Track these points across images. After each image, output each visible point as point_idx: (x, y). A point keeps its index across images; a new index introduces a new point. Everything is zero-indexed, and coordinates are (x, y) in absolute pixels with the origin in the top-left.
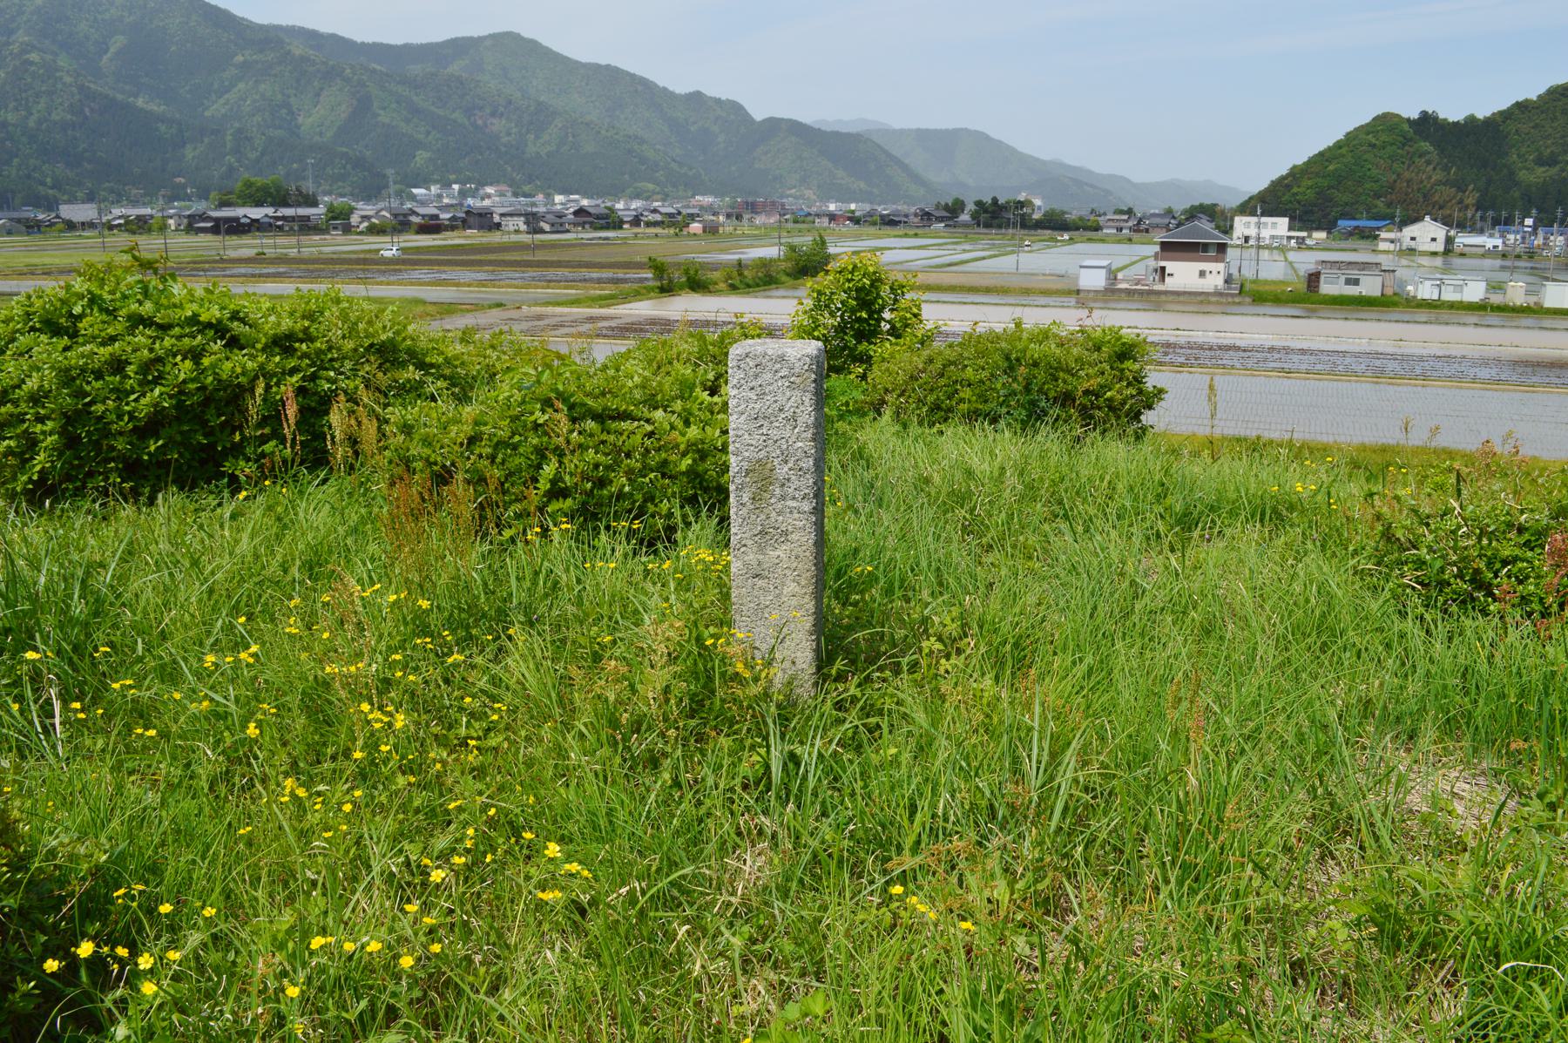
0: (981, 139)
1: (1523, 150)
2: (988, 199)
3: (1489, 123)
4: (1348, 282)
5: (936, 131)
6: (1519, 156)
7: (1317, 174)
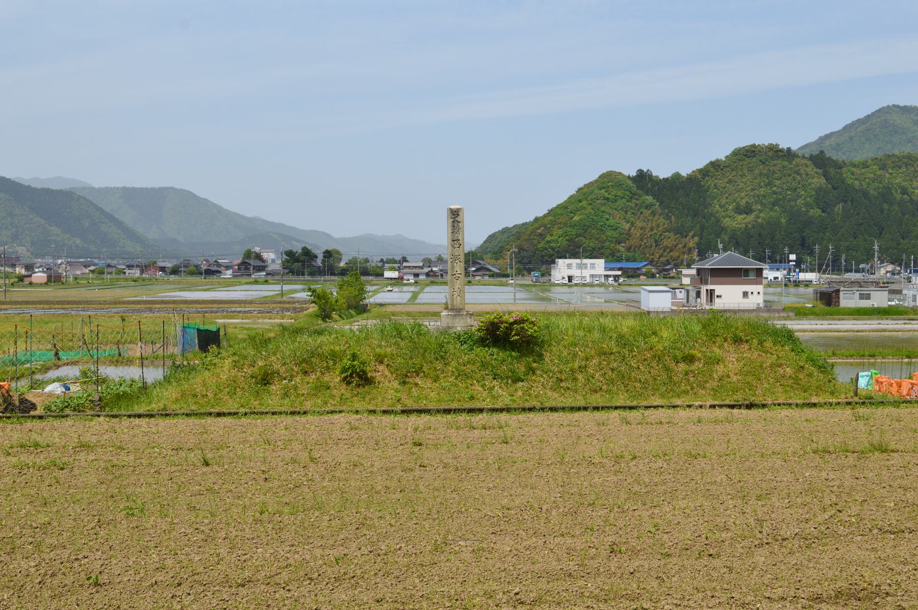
0: (188, 197)
1: (723, 201)
2: (298, 248)
3: (691, 179)
4: (862, 297)
5: (142, 190)
6: (720, 206)
7: (565, 224)
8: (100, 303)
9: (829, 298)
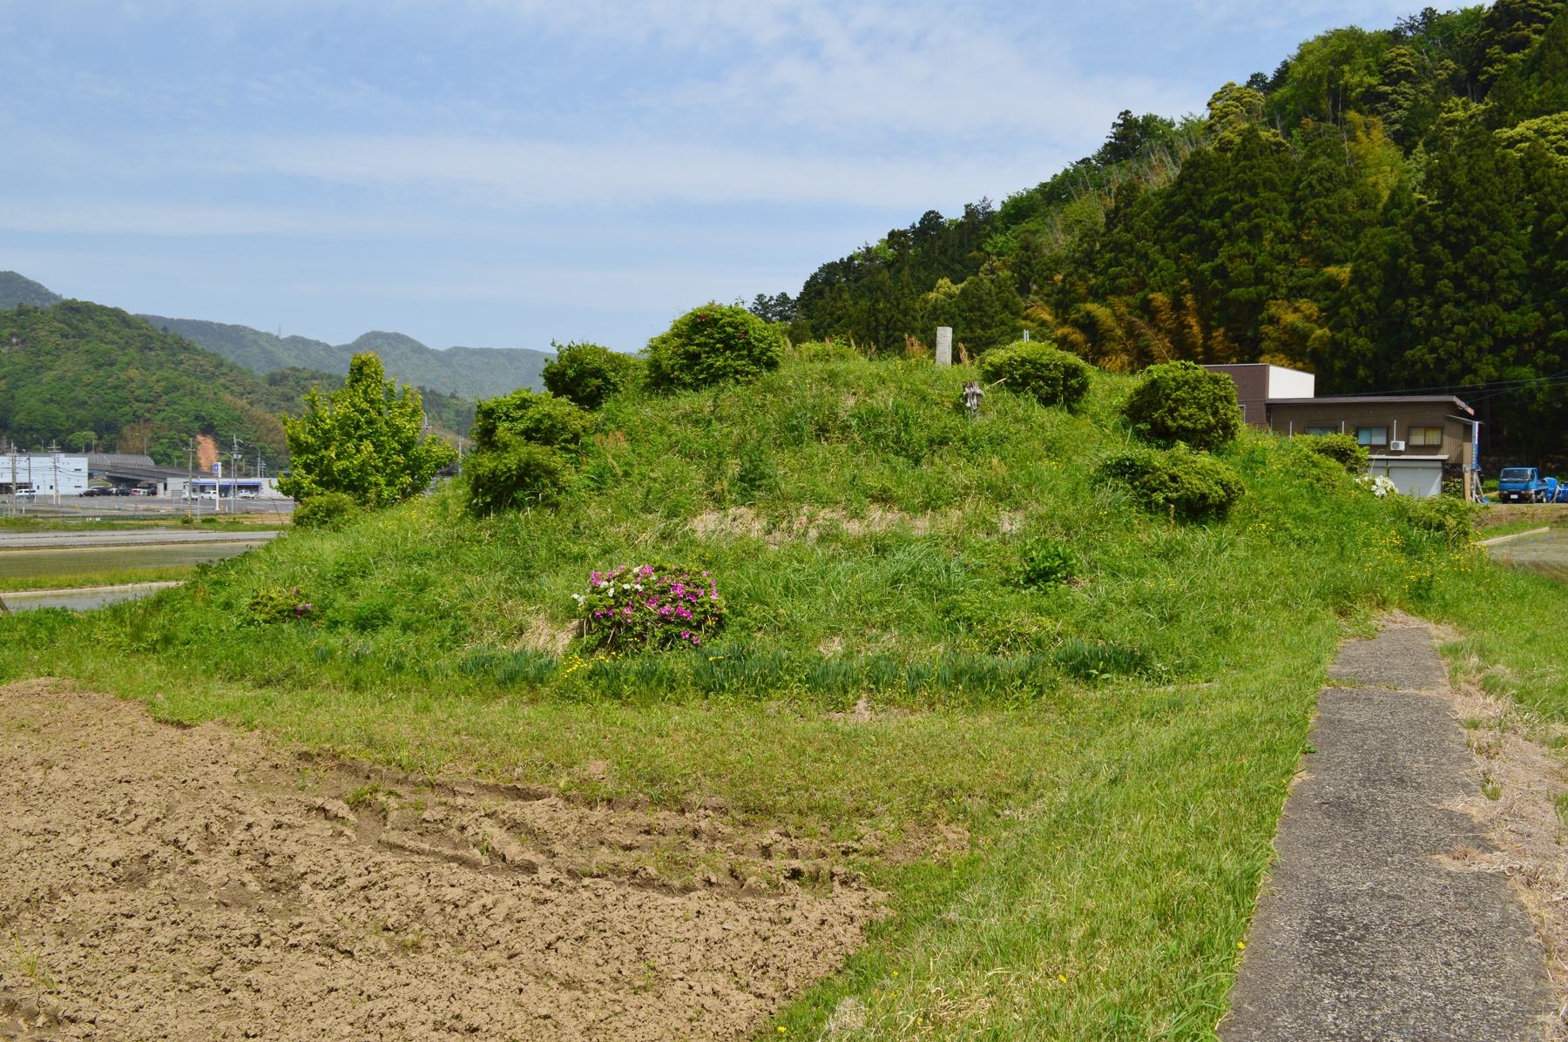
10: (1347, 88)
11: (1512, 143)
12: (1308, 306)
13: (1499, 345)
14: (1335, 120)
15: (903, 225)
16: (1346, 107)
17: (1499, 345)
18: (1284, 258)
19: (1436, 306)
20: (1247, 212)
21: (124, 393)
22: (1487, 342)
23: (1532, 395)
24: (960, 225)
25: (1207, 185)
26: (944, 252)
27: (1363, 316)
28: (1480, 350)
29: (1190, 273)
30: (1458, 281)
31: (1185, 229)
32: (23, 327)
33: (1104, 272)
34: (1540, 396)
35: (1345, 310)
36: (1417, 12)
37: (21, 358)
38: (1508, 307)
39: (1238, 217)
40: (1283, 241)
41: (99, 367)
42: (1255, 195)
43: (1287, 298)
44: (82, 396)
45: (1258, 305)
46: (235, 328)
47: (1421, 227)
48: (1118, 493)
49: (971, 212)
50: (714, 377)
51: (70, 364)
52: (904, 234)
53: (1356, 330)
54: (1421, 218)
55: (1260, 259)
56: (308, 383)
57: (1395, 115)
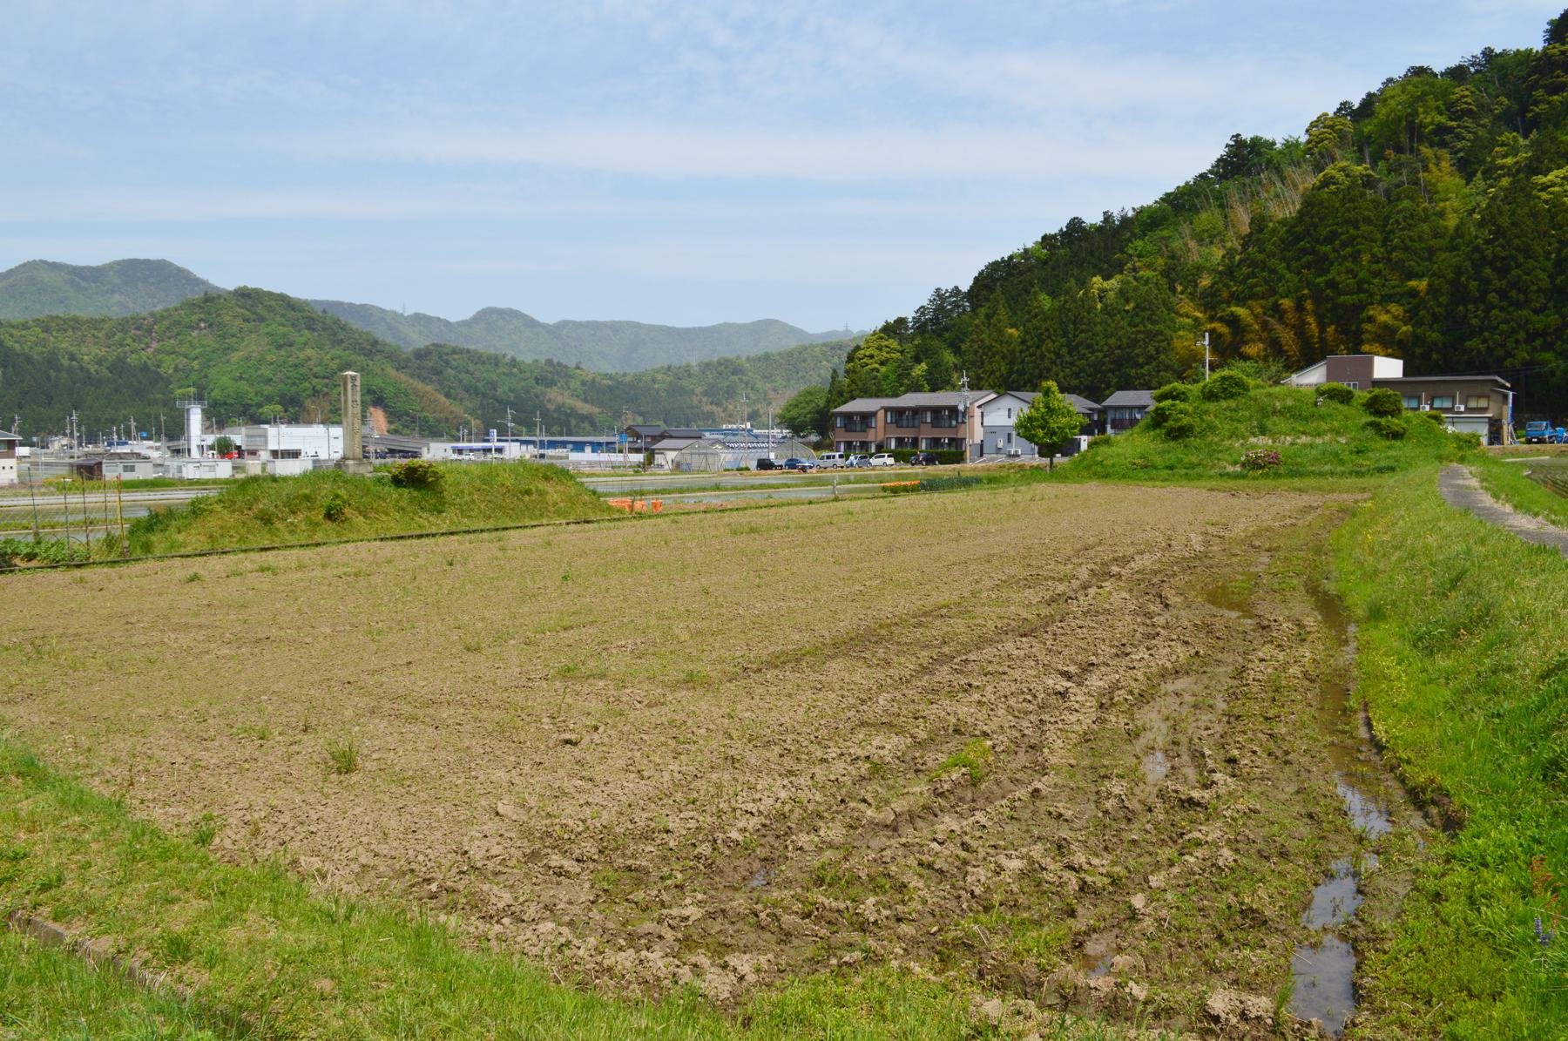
4: (126, 469)
8: (906, 489)
9: (90, 471)
10: (1422, 126)
11: (1544, 188)
12: (1395, 309)
13: (1530, 338)
14: (1412, 151)
15: (1054, 230)
16: (1420, 141)
17: (1530, 338)
18: (1378, 274)
19: (1487, 311)
20: (1351, 241)
21: (302, 371)
22: (1522, 336)
23: (1553, 373)
24: (1099, 229)
25: (1321, 219)
26: (1092, 253)
27: (1435, 318)
28: (1517, 342)
29: (1309, 284)
30: (1503, 294)
31: (1304, 251)
32: (209, 313)
33: (1244, 281)
34: (1558, 373)
35: (1422, 313)
36: (1478, 52)
37: (210, 341)
38: (1536, 312)
39: (1344, 245)
40: (1377, 262)
41: (279, 347)
42: (1357, 228)
43: (1380, 303)
44: (268, 373)
45: (1360, 307)
46: (364, 306)
47: (1477, 255)
48: (1370, 432)
49: (1108, 217)
50: (1232, 396)
51: (254, 345)
52: (1054, 237)
53: (1431, 326)
54: (1477, 249)
55: (1361, 275)
56: (450, 358)
57: (1460, 145)
